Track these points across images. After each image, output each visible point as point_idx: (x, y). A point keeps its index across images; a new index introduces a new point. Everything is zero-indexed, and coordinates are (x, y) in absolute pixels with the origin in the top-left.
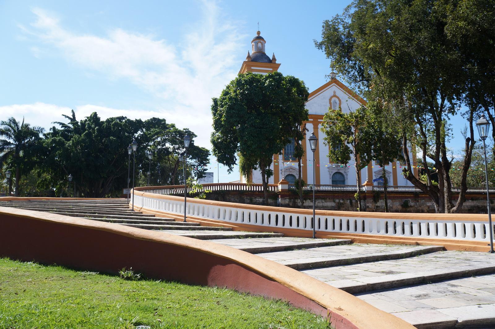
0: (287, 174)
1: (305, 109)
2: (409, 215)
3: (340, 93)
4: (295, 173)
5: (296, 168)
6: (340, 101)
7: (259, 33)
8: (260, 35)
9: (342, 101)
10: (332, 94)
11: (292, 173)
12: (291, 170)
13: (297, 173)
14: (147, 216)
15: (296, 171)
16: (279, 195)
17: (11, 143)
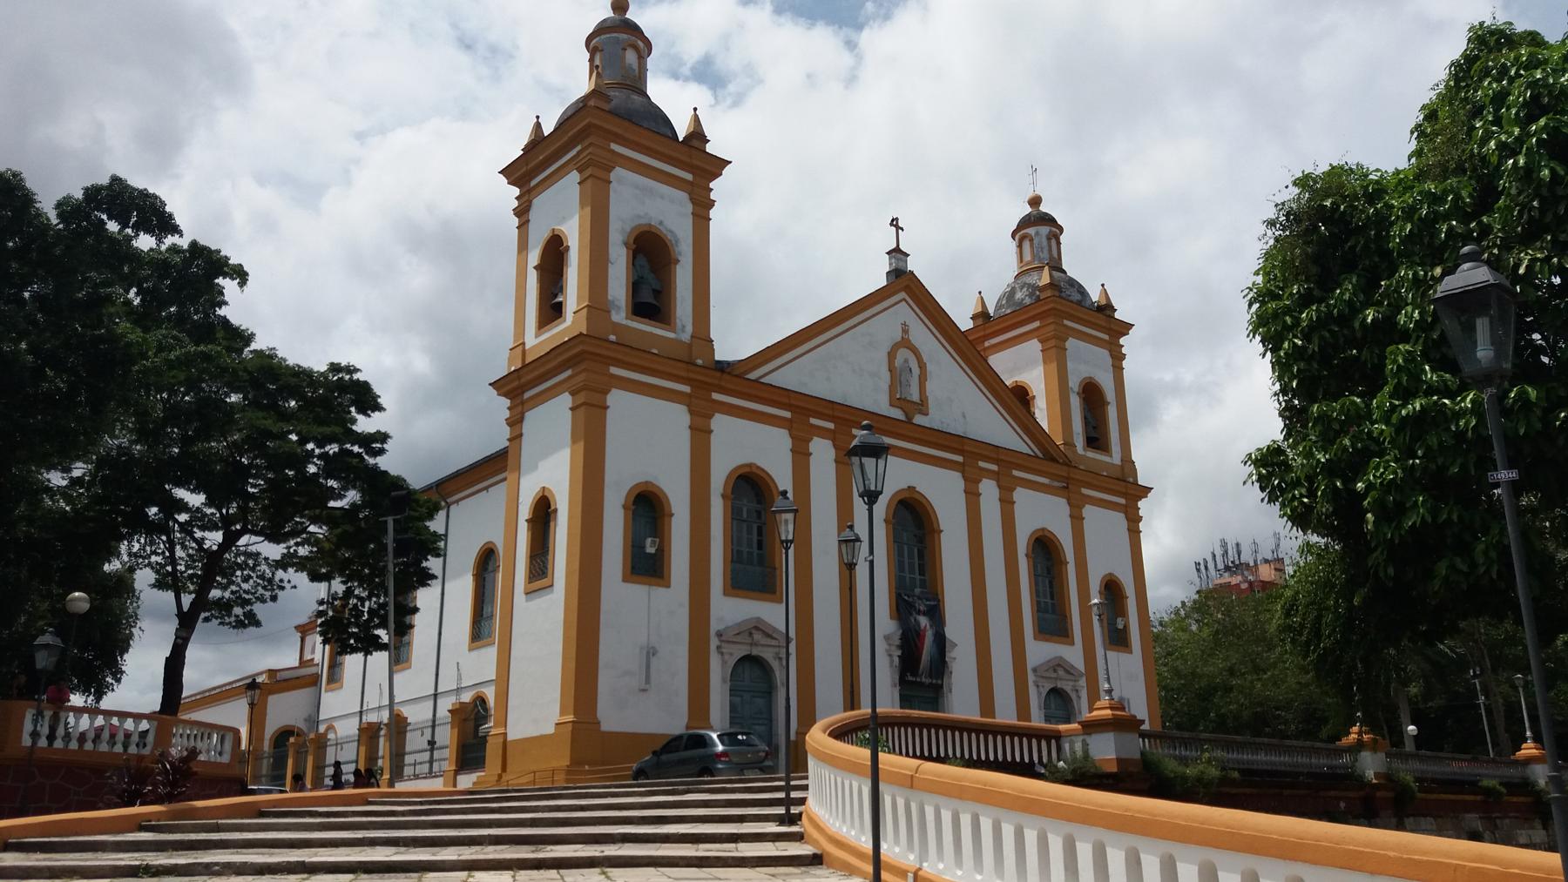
0: (740, 651)
1: (142, 233)
2: (316, 855)
3: (924, 337)
4: (771, 649)
5: (775, 630)
6: (922, 366)
7: (1035, 202)
8: (1043, 208)
9: (929, 367)
10: (898, 336)
11: (760, 648)
12: (757, 636)
13: (777, 650)
14: (353, 812)
15: (774, 643)
16: (379, 729)
17: (80, 475)
